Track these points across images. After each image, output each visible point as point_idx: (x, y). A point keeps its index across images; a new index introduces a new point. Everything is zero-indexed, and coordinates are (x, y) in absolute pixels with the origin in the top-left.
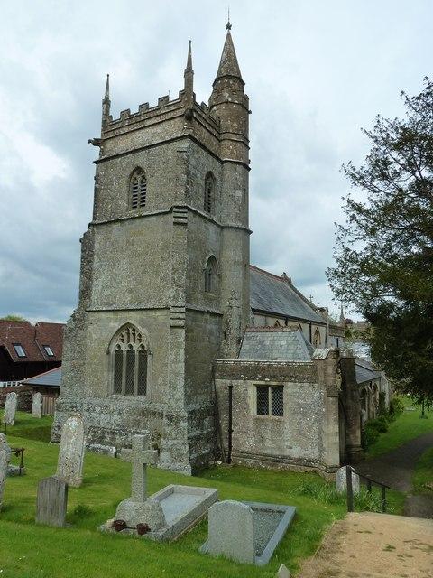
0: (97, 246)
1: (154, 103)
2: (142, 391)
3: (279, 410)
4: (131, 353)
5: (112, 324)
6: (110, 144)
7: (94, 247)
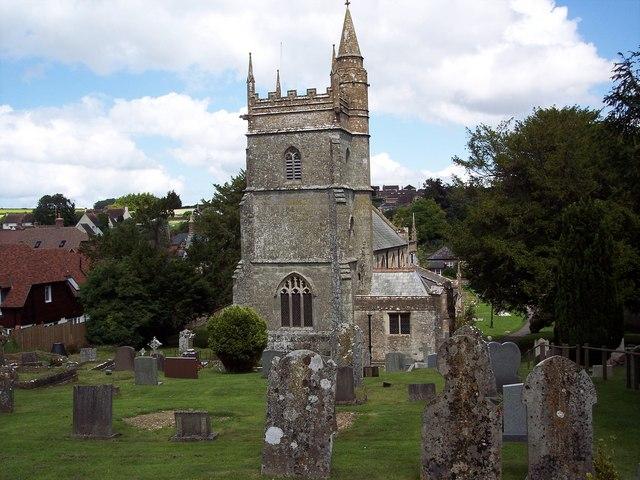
1: (302, 92)
3: (406, 329)
4: (296, 295)
5: (278, 274)
6: (259, 121)
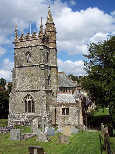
0: (17, 73)
2: (33, 111)
3: (68, 114)
4: (29, 102)
7: (16, 73)
